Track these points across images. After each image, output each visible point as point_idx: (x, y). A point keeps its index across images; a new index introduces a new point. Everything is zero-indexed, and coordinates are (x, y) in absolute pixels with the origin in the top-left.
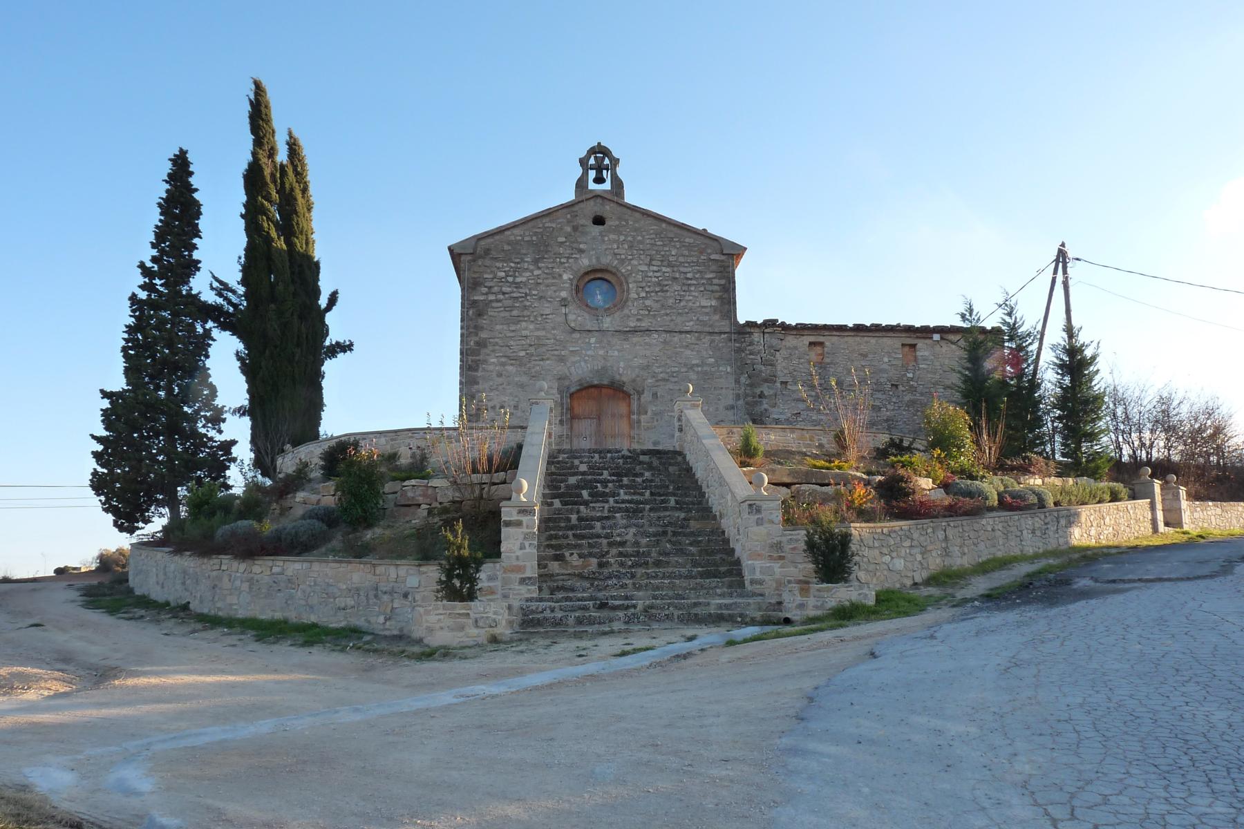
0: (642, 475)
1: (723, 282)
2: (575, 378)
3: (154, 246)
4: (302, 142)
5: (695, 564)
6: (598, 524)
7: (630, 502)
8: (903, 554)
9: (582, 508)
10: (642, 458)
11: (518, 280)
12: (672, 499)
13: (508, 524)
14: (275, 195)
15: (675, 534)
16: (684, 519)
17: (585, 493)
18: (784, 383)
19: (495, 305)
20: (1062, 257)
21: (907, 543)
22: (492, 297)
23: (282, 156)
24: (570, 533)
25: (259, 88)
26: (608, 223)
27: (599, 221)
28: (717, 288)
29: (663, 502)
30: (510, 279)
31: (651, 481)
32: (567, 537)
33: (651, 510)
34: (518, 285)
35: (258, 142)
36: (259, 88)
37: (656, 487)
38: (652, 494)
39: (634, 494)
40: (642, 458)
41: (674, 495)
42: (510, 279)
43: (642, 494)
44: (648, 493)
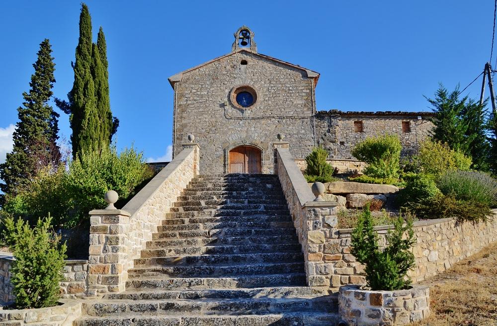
0: (247, 189)
1: (308, 91)
2: (231, 142)
3: (31, 85)
4: (105, 34)
5: (267, 260)
6: (201, 225)
7: (232, 208)
8: (437, 247)
9: (196, 213)
10: (251, 179)
11: (202, 93)
12: (262, 207)
13: (96, 230)
14: (90, 56)
15: (257, 233)
16: (267, 220)
17: (203, 203)
18: (342, 143)
19: (191, 106)
20: (487, 67)
21: (439, 238)
22: (189, 102)
23: (94, 40)
24: (177, 233)
25: (84, 8)
26: (249, 63)
27: (244, 62)
28: (304, 94)
29: (255, 207)
30: (199, 93)
31: (252, 193)
32: (175, 236)
33: (245, 214)
34: (202, 96)
35: (81, 34)
36: (84, 8)
37: (254, 197)
38: (249, 202)
39: (237, 202)
40: (251, 179)
41: (264, 202)
42: (199, 93)
43: (243, 202)
44: (246, 201)
